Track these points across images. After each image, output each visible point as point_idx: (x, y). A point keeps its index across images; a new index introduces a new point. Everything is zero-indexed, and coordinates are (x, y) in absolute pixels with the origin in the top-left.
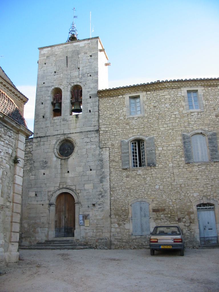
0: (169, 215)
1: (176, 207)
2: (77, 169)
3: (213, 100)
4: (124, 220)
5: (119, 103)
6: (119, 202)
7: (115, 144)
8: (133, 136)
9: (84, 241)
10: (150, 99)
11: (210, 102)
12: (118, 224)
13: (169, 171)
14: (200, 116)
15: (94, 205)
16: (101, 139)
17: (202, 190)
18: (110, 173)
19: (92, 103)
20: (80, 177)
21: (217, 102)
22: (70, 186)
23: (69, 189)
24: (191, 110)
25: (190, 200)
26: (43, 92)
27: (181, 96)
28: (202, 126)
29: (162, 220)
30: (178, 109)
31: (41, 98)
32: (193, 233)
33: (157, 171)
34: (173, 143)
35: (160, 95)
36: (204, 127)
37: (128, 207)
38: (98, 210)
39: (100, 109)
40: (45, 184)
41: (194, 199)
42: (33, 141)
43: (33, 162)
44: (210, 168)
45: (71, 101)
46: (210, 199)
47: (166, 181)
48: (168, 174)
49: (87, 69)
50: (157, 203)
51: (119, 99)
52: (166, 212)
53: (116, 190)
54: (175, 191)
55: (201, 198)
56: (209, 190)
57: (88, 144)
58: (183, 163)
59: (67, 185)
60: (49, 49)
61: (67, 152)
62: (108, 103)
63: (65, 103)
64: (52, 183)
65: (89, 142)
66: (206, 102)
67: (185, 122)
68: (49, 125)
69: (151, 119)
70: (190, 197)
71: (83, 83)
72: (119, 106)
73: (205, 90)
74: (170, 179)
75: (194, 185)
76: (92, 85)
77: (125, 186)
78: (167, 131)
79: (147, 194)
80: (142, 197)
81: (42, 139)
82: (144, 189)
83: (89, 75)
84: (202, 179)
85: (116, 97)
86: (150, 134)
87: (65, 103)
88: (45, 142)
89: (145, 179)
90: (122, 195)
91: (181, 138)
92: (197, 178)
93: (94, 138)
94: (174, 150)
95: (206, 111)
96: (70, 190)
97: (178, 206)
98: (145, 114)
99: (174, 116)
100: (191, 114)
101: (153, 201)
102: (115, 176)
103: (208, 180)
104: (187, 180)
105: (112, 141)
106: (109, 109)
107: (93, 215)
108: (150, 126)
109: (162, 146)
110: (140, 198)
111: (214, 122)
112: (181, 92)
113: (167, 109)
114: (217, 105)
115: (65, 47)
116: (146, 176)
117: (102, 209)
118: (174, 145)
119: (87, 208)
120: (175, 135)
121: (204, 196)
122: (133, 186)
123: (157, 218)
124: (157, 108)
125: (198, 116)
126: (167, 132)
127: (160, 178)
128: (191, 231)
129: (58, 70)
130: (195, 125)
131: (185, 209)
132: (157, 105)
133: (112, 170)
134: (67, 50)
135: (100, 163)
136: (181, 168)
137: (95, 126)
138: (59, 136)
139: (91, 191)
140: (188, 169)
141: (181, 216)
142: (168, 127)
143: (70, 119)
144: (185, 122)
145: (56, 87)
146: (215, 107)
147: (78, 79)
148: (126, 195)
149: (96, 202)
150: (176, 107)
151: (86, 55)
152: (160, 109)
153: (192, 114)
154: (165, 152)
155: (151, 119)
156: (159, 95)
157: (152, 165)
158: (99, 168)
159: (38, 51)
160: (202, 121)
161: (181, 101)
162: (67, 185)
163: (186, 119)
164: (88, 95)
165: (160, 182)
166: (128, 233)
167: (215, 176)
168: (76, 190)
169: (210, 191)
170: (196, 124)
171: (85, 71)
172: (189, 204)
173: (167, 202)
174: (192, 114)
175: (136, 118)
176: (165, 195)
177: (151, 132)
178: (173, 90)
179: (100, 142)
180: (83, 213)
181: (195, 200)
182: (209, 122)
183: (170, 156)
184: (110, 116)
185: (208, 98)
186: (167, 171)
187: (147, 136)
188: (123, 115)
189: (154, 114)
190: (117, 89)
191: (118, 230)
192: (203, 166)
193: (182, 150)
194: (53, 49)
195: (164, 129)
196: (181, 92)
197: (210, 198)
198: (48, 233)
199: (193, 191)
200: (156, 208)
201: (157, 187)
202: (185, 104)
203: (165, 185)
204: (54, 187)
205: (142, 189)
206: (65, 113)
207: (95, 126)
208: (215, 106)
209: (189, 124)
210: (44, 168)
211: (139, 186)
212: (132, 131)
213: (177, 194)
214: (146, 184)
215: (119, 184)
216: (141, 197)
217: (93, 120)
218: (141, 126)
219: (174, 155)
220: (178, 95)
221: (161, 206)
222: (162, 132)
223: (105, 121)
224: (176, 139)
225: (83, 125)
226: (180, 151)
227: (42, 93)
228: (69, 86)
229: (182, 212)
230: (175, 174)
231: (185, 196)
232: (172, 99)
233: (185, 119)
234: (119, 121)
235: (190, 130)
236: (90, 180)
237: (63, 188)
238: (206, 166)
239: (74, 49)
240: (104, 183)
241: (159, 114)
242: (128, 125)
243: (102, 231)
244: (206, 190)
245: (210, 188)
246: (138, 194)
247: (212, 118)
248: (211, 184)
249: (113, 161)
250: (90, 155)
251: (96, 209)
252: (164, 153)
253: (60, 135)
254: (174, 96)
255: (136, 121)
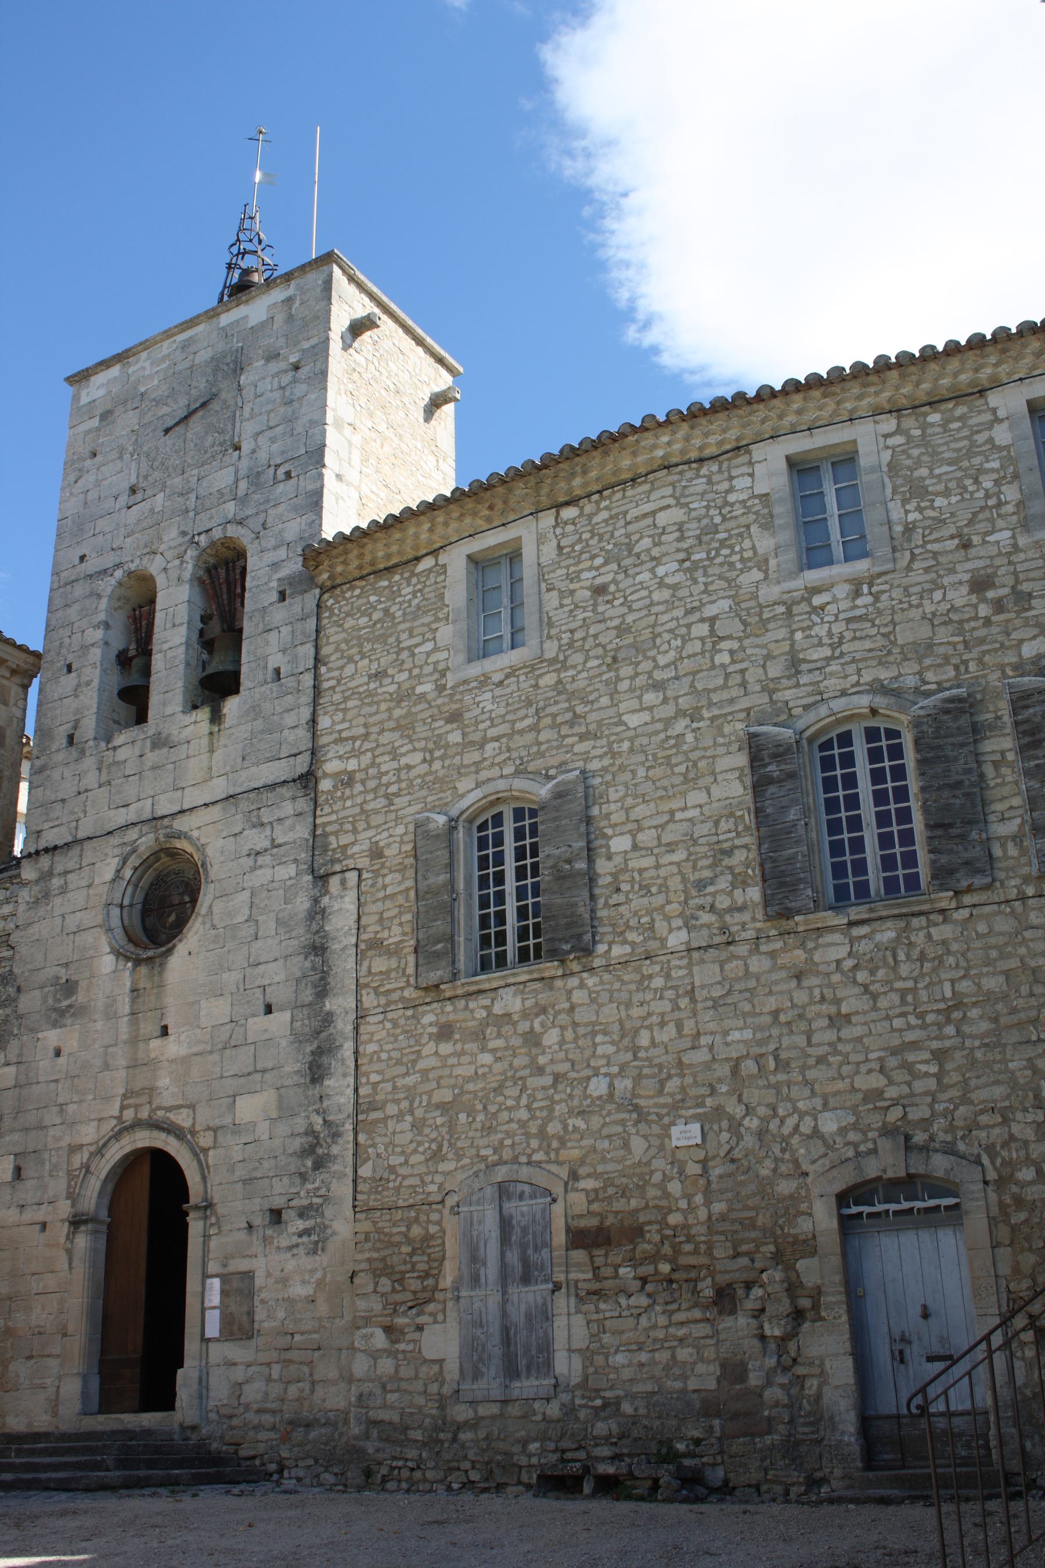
0: (665, 1268)
1: (702, 1214)
2: (202, 1013)
3: (952, 485)
4: (419, 1304)
5: (415, 602)
6: (397, 1189)
7: (389, 845)
8: (478, 785)
9: (222, 1437)
10: (577, 548)
11: (939, 502)
12: (388, 1329)
13: (668, 977)
14: (866, 606)
15: (276, 1216)
16: (325, 825)
17: (874, 1085)
18: (361, 1016)
19: (289, 628)
20: (216, 1057)
21: (981, 494)
22: (169, 1109)
23: (163, 1129)
24: (814, 576)
25: (796, 1163)
26: (76, 607)
27: (754, 497)
28: (880, 664)
29: (623, 1301)
30: (728, 581)
31: (67, 641)
32: (812, 1385)
33: (602, 983)
34: (696, 797)
35: (629, 518)
36: (894, 668)
37: (439, 1223)
38: (297, 1245)
39: (325, 651)
40: (57, 1109)
41: (822, 1150)
42: (19, 876)
43: (11, 990)
44: (929, 936)
45: (202, 633)
46: (925, 1149)
47: (653, 1043)
48: (661, 998)
49: (273, 442)
50: (596, 1191)
51: (419, 582)
52: (646, 1246)
53: (386, 1118)
54: (702, 1104)
55: (866, 1140)
56: (919, 1086)
57: (260, 860)
58: (754, 919)
59: (156, 1102)
60: (115, 371)
61: (177, 917)
62: (364, 614)
63: (165, 646)
64: (91, 1097)
65: (266, 850)
66: (908, 507)
67: (768, 657)
68: (91, 780)
69: (574, 667)
70: (795, 1141)
71: (250, 522)
72: (414, 619)
73: (906, 433)
74: (671, 1030)
75: (821, 1060)
76: (294, 528)
77: (430, 1094)
78: (659, 726)
79: (542, 1133)
80: (516, 1157)
81: (62, 863)
82: (528, 1107)
83: (281, 471)
84: (873, 1015)
85: (402, 574)
86: (565, 763)
87: (165, 646)
88: (70, 876)
89: (533, 1039)
90: (415, 1151)
91: (742, 760)
92: (845, 1009)
93: (288, 823)
94: (702, 841)
95: (909, 568)
96: (168, 1131)
97: (719, 1207)
98: (548, 644)
99: (703, 629)
100: (809, 601)
101: (574, 1176)
102: (384, 1033)
103: (913, 1020)
104: (775, 1032)
105: (377, 827)
106: (367, 647)
107: (269, 1275)
108: (568, 710)
109: (630, 826)
110: (506, 1163)
111: (961, 632)
112: (752, 475)
113: (666, 594)
114: (981, 516)
115: (184, 346)
116: (542, 1025)
117: (314, 1238)
118: (702, 814)
119: (242, 1236)
120: (705, 749)
121: (887, 1131)
122: (470, 1087)
123: (595, 1286)
124: (613, 594)
125: (857, 607)
126: (662, 736)
127: (616, 1027)
128: (800, 1370)
129: (146, 477)
130: (835, 667)
131: (760, 1220)
132: (614, 581)
133: (369, 1000)
134: (191, 357)
135: (314, 968)
136: (742, 950)
137: (295, 755)
138: (133, 834)
139: (263, 1130)
140: (783, 959)
141: (733, 1270)
142: (665, 701)
143: (187, 733)
144: (768, 657)
145: (133, 567)
146: (966, 530)
147: (230, 508)
148: (434, 1146)
149: (284, 1199)
150: (717, 570)
151: (274, 367)
152: (625, 598)
153: (817, 600)
154: (648, 862)
155: (574, 667)
156: (625, 513)
157: (570, 952)
158: (307, 995)
159: (69, 390)
160: (883, 635)
161: (748, 527)
162: (156, 1102)
163: (782, 633)
164: (274, 584)
165: (618, 1051)
166: (434, 1388)
167: (965, 986)
168: (193, 1133)
169: (933, 1095)
170: (843, 661)
171: (263, 456)
172: (785, 1187)
173: (657, 1177)
174: (817, 600)
175: (497, 677)
176: (645, 1137)
177: (576, 749)
178: (704, 471)
179: (317, 842)
180: (225, 1266)
181: (826, 1162)
182: (924, 632)
183: (675, 883)
184: (372, 686)
185: (924, 479)
186: (658, 982)
187: (552, 772)
188: (435, 670)
189: (596, 636)
190: (390, 522)
191: (386, 1366)
192: (876, 925)
193: (746, 840)
194: (130, 371)
195: (645, 716)
196: (752, 475)
197: (932, 1138)
198: (58, 1392)
199: (818, 1102)
200: (593, 1222)
201: (598, 1087)
202: (772, 547)
203: (645, 1071)
204: (95, 1123)
205: (518, 1107)
206: (164, 705)
207: (295, 755)
208: (971, 522)
209: (795, 663)
210: (58, 1016)
211: (499, 1090)
212: (476, 756)
213: (716, 1127)
214: (540, 1071)
215: (400, 1082)
216: (507, 1154)
217: (290, 720)
218: (523, 719)
219: (697, 875)
220: (732, 498)
221: (619, 1205)
222: (631, 740)
223: (343, 721)
224: (713, 773)
225: (243, 759)
226: (737, 842)
227: (73, 612)
228: (189, 552)
229: (743, 1241)
230: (700, 995)
231: (761, 1134)
232: (693, 530)
233: (771, 636)
234: (413, 710)
235: (805, 701)
236: (264, 1071)
237: (137, 1124)
238: (902, 924)
239: (221, 346)
240: (327, 1083)
241: (622, 630)
242: (455, 725)
243: (311, 1375)
244: (905, 1090)
245: (927, 1074)
246: (495, 1138)
247: (944, 607)
248: (935, 1045)
249: (376, 944)
250: (268, 924)
251: (284, 1242)
252: (641, 871)
253: (137, 829)
254: (708, 507)
255: (498, 692)
